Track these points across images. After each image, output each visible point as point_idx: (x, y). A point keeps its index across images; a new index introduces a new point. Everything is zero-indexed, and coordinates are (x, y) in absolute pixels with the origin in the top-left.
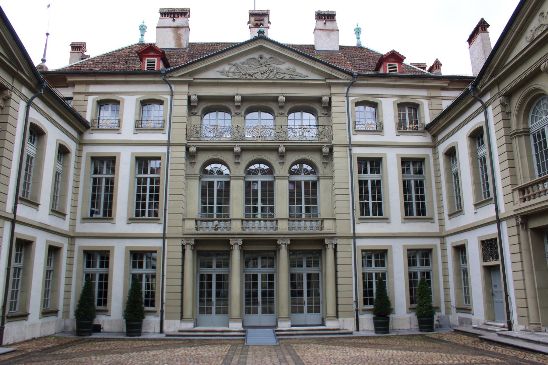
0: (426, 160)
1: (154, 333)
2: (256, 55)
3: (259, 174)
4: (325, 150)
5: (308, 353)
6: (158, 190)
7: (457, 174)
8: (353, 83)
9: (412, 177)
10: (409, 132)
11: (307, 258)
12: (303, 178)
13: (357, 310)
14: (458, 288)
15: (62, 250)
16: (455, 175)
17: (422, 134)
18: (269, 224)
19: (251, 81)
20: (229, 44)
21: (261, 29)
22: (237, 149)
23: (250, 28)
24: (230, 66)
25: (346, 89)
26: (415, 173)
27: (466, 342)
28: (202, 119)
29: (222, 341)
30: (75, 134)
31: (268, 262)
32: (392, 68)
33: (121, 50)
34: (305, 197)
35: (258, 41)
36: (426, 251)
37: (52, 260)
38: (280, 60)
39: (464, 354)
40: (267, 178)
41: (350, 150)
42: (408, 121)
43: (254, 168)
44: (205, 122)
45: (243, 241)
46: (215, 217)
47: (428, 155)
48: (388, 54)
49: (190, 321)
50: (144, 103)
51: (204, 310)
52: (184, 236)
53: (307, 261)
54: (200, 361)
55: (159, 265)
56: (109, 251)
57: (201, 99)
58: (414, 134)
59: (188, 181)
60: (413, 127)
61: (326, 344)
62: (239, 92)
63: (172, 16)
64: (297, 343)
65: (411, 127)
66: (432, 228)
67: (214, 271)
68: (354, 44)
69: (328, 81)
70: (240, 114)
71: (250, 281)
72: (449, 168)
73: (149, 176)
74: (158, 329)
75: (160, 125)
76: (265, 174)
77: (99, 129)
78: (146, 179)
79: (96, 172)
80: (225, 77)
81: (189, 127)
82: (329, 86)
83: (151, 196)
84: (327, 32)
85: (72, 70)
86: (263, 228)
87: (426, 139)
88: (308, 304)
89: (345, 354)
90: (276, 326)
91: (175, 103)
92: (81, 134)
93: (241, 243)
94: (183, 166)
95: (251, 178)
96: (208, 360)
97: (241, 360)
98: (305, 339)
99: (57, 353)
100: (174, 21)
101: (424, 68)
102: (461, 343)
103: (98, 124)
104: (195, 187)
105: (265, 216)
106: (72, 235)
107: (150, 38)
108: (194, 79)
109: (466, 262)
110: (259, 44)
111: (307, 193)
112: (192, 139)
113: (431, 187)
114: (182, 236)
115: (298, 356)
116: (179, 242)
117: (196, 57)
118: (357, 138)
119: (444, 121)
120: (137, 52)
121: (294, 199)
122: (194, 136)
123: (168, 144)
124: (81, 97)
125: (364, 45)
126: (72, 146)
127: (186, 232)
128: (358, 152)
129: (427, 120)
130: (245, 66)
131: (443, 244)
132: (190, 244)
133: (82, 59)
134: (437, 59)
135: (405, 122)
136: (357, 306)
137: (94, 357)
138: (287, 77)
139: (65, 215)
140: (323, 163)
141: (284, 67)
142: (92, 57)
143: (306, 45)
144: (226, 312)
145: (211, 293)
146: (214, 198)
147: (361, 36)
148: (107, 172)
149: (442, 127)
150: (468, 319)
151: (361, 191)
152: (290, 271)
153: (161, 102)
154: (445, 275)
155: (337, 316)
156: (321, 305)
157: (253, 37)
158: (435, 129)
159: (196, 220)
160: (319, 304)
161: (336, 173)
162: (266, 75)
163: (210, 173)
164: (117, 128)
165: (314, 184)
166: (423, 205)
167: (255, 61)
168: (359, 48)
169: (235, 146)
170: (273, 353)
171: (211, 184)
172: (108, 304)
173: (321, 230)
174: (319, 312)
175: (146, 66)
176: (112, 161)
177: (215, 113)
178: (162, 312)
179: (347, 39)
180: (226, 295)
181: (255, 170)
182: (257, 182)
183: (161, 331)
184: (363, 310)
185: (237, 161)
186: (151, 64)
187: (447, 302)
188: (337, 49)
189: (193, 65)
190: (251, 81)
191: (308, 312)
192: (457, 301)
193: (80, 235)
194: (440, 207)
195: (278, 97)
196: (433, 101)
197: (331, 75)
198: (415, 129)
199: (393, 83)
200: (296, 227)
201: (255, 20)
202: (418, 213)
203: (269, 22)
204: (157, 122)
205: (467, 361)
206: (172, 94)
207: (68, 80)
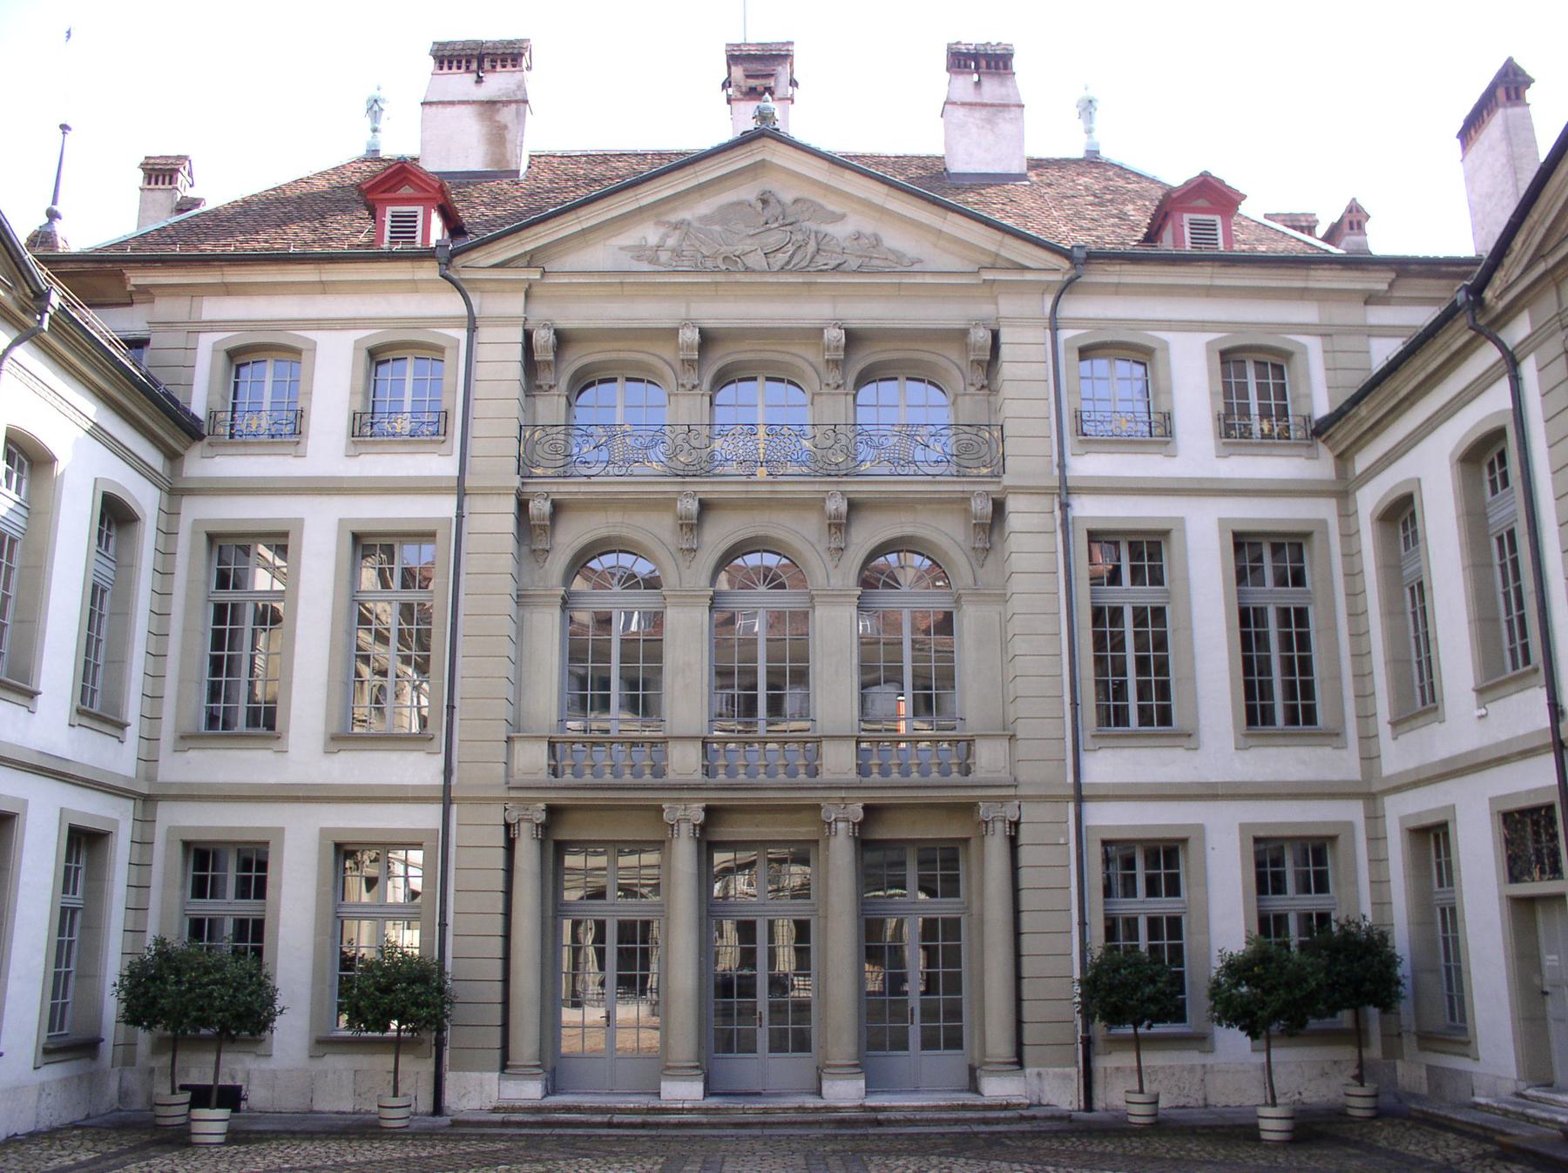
7: (1420, 585)
9: (1271, 597)
15: (112, 839)
23: (729, 101)
24: (662, 230)
26: (1281, 581)
27: (1452, 1156)
28: (569, 404)
30: (155, 459)
32: (1203, 232)
35: (755, 145)
40: (786, 600)
42: (1254, 409)
47: (1324, 522)
56: (267, 843)
60: (1272, 430)
63: (474, 66)
65: (1266, 427)
66: (1340, 764)
68: (1079, 153)
74: (425, 1104)
79: (223, 581)
80: (646, 267)
84: (984, 112)
87: (1318, 466)
91: (481, 352)
100: (479, 80)
101: (1310, 230)
104: (548, 628)
106: (144, 789)
107: (399, 142)
109: (1451, 883)
114: (502, 793)
118: (1086, 466)
122: (544, 462)
125: (1107, 153)
126: (144, 497)
133: (180, 211)
135: (1245, 411)
155: (1019, 1062)
161: (1018, 584)
168: (1092, 161)
179: (1049, 132)
196: (1341, 343)
201: (747, 77)
202: (1292, 719)
207: (133, 281)
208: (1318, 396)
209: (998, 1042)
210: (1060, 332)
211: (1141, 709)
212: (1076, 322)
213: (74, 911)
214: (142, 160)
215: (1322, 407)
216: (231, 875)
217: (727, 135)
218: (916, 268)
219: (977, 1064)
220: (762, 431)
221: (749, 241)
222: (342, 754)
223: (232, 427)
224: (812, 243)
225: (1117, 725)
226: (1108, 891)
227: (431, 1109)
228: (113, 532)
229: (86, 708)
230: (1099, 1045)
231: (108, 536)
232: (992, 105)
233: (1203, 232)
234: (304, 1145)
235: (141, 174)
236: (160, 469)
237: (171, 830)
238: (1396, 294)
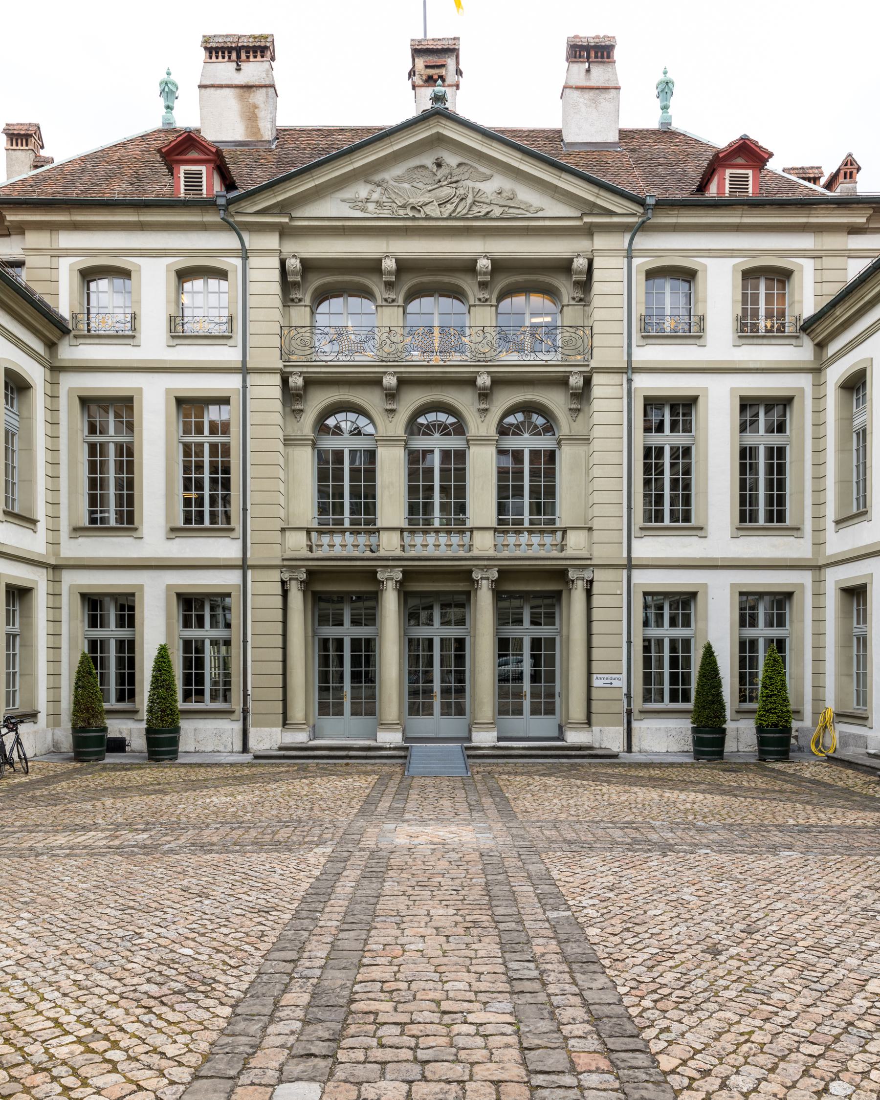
0: (796, 402)
1: (232, 752)
2: (428, 160)
3: (437, 435)
4: (576, 381)
5: (527, 792)
6: (227, 470)
7: (864, 431)
8: (643, 222)
9: (762, 439)
10: (763, 337)
11: (532, 608)
12: (526, 443)
13: (629, 713)
14: (843, 672)
15: (34, 593)
16: (858, 434)
17: (793, 341)
18: (455, 539)
19: (416, 223)
20: (368, 130)
21: (439, 89)
22: (390, 381)
23: (414, 87)
24: (370, 187)
25: (627, 237)
26: (770, 430)
27: (850, 783)
28: (313, 313)
29: (363, 769)
30: (38, 346)
31: (453, 613)
32: (739, 182)
33: (124, 145)
34: (530, 488)
35: (432, 121)
36: (778, 597)
37: (17, 614)
38: (482, 169)
39: (843, 807)
40: (453, 443)
41: (630, 381)
42: (762, 312)
43: (425, 422)
44: (321, 320)
45: (404, 572)
46: (347, 524)
47: (802, 390)
48: (730, 146)
49: (302, 730)
50: (184, 275)
51: (328, 706)
52: (286, 563)
53: (532, 613)
54: (316, 807)
55: (235, 618)
56: (133, 595)
57: (309, 266)
58: (773, 341)
59: (290, 450)
60: (772, 326)
61: (565, 777)
62: (391, 250)
63: (234, 56)
64: (509, 773)
65: (769, 325)
66: (796, 548)
67: (348, 632)
68: (654, 125)
69: (587, 219)
70: (393, 301)
71: (417, 653)
72: (846, 419)
73: (206, 438)
74: (238, 746)
75: (224, 327)
76: (448, 434)
77: (91, 336)
78: (201, 445)
79: (92, 430)
80: (358, 214)
81: (286, 331)
82: (589, 231)
83: (214, 481)
84: (592, 93)
85: (15, 195)
86: (443, 547)
87: (802, 352)
88: (532, 697)
89: (599, 797)
90: (469, 739)
91: (252, 275)
92: (51, 346)
93: (399, 576)
94: (278, 419)
95: (421, 443)
96: (332, 805)
97: (396, 805)
98: (523, 765)
99: (38, 793)
100: (238, 69)
101: (815, 180)
102: (840, 784)
103: (88, 324)
104: (305, 462)
105: (448, 523)
106: (53, 562)
107: (187, 117)
108: (292, 218)
109: (865, 622)
110: (434, 131)
111: (534, 473)
112: (293, 358)
113: (802, 460)
114: (279, 562)
115: (507, 799)
116: (276, 575)
117: (292, 164)
118: (645, 354)
119: (847, 310)
120: (159, 151)
121: (507, 487)
122: (297, 352)
123: (244, 370)
124: (43, 261)
125: (677, 125)
126: (34, 373)
127: (289, 554)
128: (646, 384)
129: (808, 308)
130: (406, 189)
131: (818, 582)
132: (297, 579)
133: (36, 167)
134: (850, 155)
135: (755, 314)
136: (629, 704)
137: (112, 800)
138: (497, 212)
139: (34, 522)
140: (570, 409)
141: (493, 185)
142: (58, 161)
143: (543, 131)
144: (371, 712)
145: (345, 673)
146: (345, 489)
147: (673, 102)
148: (118, 431)
149: (842, 324)
150: (860, 736)
151: (647, 469)
152: (497, 632)
153: (221, 274)
154: (818, 648)
155: (589, 723)
156: (557, 699)
157: (420, 113)
158: (821, 328)
159: (309, 531)
160: (553, 696)
161: (597, 432)
162: (450, 207)
163: (334, 433)
164: (130, 333)
165: (551, 456)
166: (781, 501)
167: (425, 173)
168: (666, 133)
169: (385, 373)
170: (461, 793)
171: (338, 456)
172: (137, 698)
173: (562, 550)
174: (554, 714)
175: (182, 187)
176: (124, 405)
177: (341, 300)
178: (245, 711)
179: (639, 113)
180: (370, 679)
181: (428, 427)
182: (433, 451)
183: (245, 749)
184: (641, 712)
185: (389, 407)
186: (193, 181)
187: (818, 700)
188: (614, 137)
189: (287, 184)
190: (416, 223)
191: (532, 714)
192: (839, 700)
193: (72, 563)
194: (818, 504)
195: (475, 261)
196: (828, 262)
197: (594, 205)
198: (778, 330)
199: (737, 220)
200: (512, 546)
201: (427, 67)
202: (770, 518)
203: (459, 72)
204: (217, 320)
205: (848, 822)
206: (245, 254)
207: (9, 218)
208: (806, 299)
209: (577, 711)
210: (634, 260)
211: (672, 512)
212: (645, 252)
213: (15, 636)
214: (4, 126)
215: (808, 310)
216: (112, 616)
217: (411, 112)
218: (540, 214)
219: (564, 724)
220: (436, 332)
221: (428, 195)
222: (177, 540)
223: (88, 324)
224: (470, 196)
225: (750, 522)
226: (646, 624)
227: (241, 750)
228: (15, 396)
229: (10, 510)
230: (635, 714)
231: (12, 399)
232: (598, 88)
233: (739, 182)
234: (166, 770)
235: (4, 137)
236: (42, 353)
237: (71, 587)
238: (871, 226)
